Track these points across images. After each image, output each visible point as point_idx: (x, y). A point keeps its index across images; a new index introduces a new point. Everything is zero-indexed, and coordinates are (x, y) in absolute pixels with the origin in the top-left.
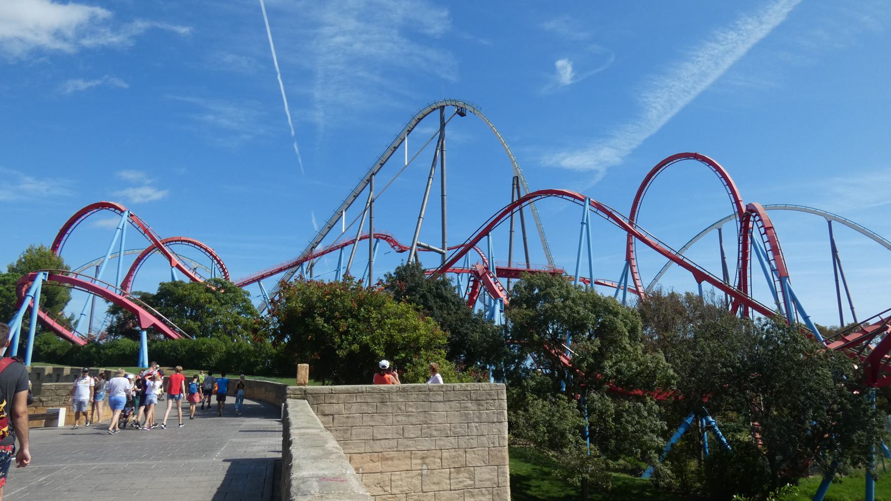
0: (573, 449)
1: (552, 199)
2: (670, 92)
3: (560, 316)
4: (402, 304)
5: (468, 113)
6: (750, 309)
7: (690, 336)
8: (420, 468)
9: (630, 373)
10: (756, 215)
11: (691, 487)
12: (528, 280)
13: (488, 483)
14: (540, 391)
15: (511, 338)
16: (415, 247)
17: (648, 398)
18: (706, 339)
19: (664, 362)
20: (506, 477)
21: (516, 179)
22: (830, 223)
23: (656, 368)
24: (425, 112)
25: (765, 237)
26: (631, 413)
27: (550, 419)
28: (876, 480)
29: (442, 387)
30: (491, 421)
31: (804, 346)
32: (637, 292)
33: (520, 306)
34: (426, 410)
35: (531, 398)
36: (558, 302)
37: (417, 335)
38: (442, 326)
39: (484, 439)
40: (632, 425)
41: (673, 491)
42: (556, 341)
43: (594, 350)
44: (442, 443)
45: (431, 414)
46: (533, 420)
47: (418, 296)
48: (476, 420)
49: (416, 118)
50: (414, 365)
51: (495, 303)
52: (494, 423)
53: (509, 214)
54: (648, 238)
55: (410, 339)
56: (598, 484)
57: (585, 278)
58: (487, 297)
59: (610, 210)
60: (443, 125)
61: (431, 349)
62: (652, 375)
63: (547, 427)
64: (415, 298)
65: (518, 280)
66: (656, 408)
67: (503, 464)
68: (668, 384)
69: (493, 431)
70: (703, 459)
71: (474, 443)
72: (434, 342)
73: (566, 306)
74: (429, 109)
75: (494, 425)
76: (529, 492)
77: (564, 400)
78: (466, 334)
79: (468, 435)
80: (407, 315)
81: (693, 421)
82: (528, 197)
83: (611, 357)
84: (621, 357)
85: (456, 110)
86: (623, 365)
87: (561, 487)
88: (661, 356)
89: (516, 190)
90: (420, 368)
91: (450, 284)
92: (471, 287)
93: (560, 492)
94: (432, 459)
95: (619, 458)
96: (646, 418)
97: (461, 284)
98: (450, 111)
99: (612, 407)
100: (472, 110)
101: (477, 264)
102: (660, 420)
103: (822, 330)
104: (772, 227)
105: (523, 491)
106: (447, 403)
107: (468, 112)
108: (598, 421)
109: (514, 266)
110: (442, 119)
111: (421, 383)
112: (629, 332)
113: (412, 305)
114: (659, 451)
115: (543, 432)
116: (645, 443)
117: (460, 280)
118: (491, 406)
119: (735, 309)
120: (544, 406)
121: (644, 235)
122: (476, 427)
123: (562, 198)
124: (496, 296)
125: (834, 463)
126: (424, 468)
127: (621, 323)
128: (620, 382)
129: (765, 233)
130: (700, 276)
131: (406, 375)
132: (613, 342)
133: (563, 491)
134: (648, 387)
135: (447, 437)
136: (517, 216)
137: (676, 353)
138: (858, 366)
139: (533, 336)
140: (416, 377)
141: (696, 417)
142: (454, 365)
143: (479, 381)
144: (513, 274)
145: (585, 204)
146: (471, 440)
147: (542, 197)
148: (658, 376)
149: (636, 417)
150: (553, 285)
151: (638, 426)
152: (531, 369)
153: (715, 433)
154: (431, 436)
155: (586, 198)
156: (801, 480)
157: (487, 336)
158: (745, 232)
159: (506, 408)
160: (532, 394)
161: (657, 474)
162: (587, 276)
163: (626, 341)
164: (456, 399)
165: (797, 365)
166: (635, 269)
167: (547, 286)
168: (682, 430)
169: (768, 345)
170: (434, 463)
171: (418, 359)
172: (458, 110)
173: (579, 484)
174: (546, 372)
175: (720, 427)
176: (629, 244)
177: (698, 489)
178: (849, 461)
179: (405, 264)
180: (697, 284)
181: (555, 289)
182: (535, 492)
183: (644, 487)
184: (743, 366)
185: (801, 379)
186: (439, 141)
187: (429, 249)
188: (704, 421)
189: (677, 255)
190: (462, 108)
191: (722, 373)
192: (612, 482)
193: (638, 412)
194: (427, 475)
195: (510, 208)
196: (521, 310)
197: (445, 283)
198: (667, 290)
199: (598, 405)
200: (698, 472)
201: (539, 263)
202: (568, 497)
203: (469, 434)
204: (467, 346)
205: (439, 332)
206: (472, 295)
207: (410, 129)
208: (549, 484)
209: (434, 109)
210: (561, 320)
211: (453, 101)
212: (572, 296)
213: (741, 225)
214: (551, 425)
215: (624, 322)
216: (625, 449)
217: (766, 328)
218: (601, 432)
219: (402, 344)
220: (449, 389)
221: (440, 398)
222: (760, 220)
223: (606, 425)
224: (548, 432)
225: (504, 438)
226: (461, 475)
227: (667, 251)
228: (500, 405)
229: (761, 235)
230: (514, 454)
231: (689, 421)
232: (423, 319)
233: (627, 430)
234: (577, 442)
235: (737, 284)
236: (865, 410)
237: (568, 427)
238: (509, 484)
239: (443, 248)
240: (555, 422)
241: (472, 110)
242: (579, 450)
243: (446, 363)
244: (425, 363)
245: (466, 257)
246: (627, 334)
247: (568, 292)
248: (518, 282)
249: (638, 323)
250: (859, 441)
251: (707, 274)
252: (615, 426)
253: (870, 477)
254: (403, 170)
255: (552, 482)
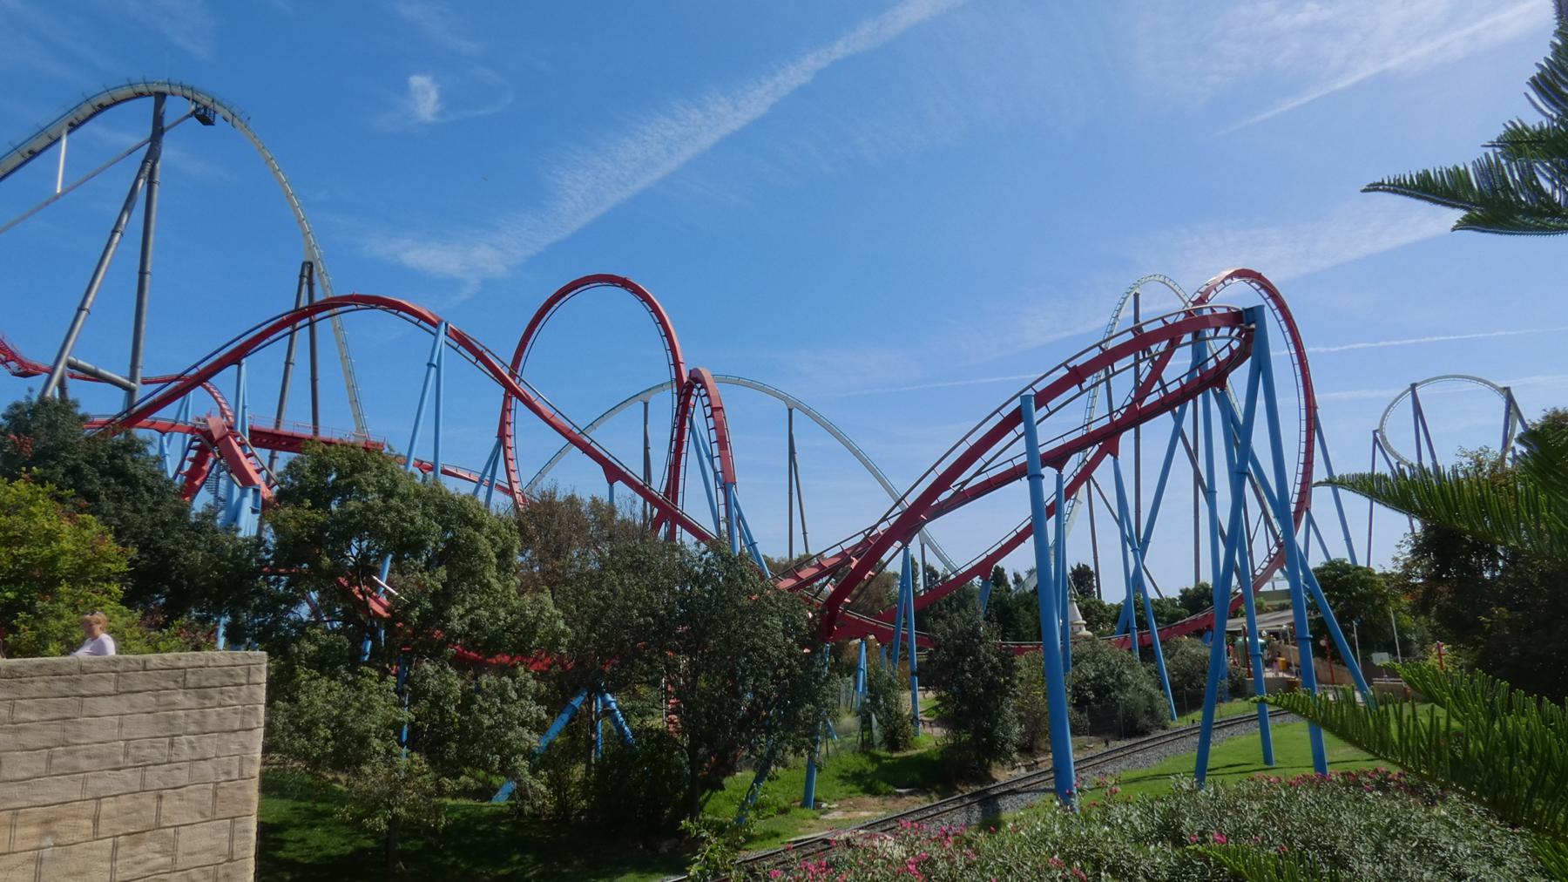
0: (380, 765)
1: (378, 314)
2: (597, 178)
3: (376, 526)
4: (20, 484)
5: (218, 119)
6: (678, 527)
7: (594, 566)
8: (34, 844)
9: (494, 628)
10: (702, 387)
11: (572, 809)
12: (319, 455)
13: (208, 855)
14: (323, 663)
15: (272, 562)
16: (61, 367)
17: (521, 669)
18: (619, 572)
19: (552, 609)
20: (249, 838)
21: (309, 266)
22: (790, 410)
23: (538, 619)
24: (119, 94)
25: (710, 420)
26: (489, 695)
27: (341, 713)
28: (820, 770)
29: (116, 662)
30: (228, 728)
31: (753, 586)
32: (510, 492)
33: (299, 504)
34: (68, 715)
35: (307, 677)
36: (374, 499)
37: (52, 551)
38: (118, 534)
39: (207, 767)
40: (490, 714)
41: (544, 818)
42: (365, 569)
43: (436, 588)
44: (99, 783)
45: (80, 723)
46: (306, 718)
47: (60, 470)
48: (193, 728)
49: (96, 102)
50: (38, 617)
51: (243, 495)
52: (234, 731)
53: (288, 329)
54: (539, 404)
55: (32, 560)
56: (419, 822)
57: (422, 462)
58: (223, 483)
59: (481, 349)
60: (158, 131)
61: (86, 583)
62: (531, 630)
63: (332, 729)
64: (52, 474)
65: (296, 455)
66: (532, 684)
67: (246, 813)
68: (555, 643)
69: (229, 749)
70: (593, 761)
71: (182, 776)
72: (96, 567)
73: (388, 509)
74: (128, 92)
75: (233, 735)
76: (281, 854)
77: (371, 677)
78: (175, 553)
79: (170, 762)
80: (32, 508)
81: (584, 703)
82: (330, 304)
83: (463, 600)
84: (481, 599)
85: (193, 108)
86: (484, 613)
87: (346, 836)
88: (547, 598)
89: (305, 288)
90: (52, 622)
91: (145, 450)
92: (190, 460)
93: (343, 845)
94: (71, 822)
95: (462, 773)
96: (514, 702)
97: (173, 456)
98: (176, 108)
99: (457, 684)
100: (229, 116)
101: (209, 416)
102: (537, 705)
103: (768, 561)
104: (722, 408)
105: (269, 852)
106: (124, 697)
107: (218, 119)
108: (429, 713)
109: (285, 429)
110: (158, 119)
111: (52, 655)
112: (498, 557)
113: (47, 489)
114: (529, 754)
115: (323, 738)
116: (508, 744)
117: (165, 443)
118: (230, 697)
119: (657, 526)
120: (331, 690)
121: (533, 397)
122: (190, 743)
123: (396, 314)
124: (247, 481)
125: (772, 752)
126: (44, 844)
127: (485, 541)
128: (474, 643)
129: (712, 416)
130: (614, 473)
131: (14, 638)
132: (470, 574)
133: (350, 843)
134: (521, 650)
135: (118, 769)
136: (302, 336)
137: (570, 593)
138: (813, 614)
139: (321, 559)
140: (40, 643)
141: (589, 696)
142: (138, 614)
143: (197, 648)
144: (284, 443)
145: (438, 332)
146: (176, 771)
147: (360, 307)
148: (541, 632)
149: (498, 701)
150: (367, 468)
151: (500, 716)
152: (308, 621)
153: (615, 720)
154: (75, 771)
155: (440, 322)
156: (727, 781)
157: (222, 557)
158: (683, 412)
159: (263, 700)
160: (308, 668)
161: (521, 793)
162: (429, 458)
163: (491, 576)
164: (150, 687)
165: (741, 612)
166: (510, 454)
167: (353, 470)
168: (565, 717)
169: (706, 582)
170: (76, 829)
171: (51, 603)
172: (197, 110)
173: (384, 827)
174: (332, 626)
175: (619, 708)
176: (506, 410)
177: (583, 811)
178: (790, 748)
179: (35, 399)
180: (608, 485)
181: (370, 476)
182: (294, 851)
183: (497, 817)
184: (669, 614)
185: (743, 634)
186: (145, 162)
187: (96, 377)
188: (599, 700)
189: (581, 436)
190: (205, 107)
191: (639, 625)
192: (446, 815)
193: (502, 694)
194: (53, 859)
195: (290, 321)
196: (300, 511)
197: (132, 447)
198: (565, 490)
199: (433, 683)
200: (584, 784)
201: (338, 426)
202: (361, 851)
203: (174, 758)
204: (174, 577)
205: (110, 547)
206: (192, 475)
207: (76, 122)
208: (324, 832)
209: (141, 95)
210: (376, 532)
211: (188, 89)
212: (400, 490)
213: (679, 401)
214: (341, 724)
215: (491, 540)
216: (473, 757)
217: (704, 557)
218: (433, 732)
219: (11, 571)
220: (134, 666)
221: (109, 687)
222: (707, 395)
223: (442, 719)
224: (335, 737)
225: (252, 761)
226: (141, 849)
227: (567, 429)
228: (251, 696)
229: (706, 418)
230: (270, 787)
231: (577, 702)
232: (71, 517)
233: (480, 724)
234: (389, 751)
235: (663, 490)
236: (817, 675)
237: (374, 726)
238: (252, 852)
239: (133, 378)
240: (349, 719)
241: (229, 116)
242: (390, 767)
243: (118, 611)
244: (67, 613)
245: (182, 404)
246: (495, 560)
247: (395, 483)
248: (298, 458)
249: (514, 542)
250: (807, 718)
251: (624, 470)
252: (459, 719)
253: (812, 766)
254: (47, 203)
255: (331, 828)
